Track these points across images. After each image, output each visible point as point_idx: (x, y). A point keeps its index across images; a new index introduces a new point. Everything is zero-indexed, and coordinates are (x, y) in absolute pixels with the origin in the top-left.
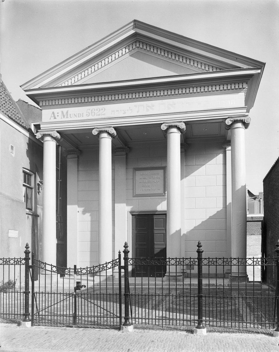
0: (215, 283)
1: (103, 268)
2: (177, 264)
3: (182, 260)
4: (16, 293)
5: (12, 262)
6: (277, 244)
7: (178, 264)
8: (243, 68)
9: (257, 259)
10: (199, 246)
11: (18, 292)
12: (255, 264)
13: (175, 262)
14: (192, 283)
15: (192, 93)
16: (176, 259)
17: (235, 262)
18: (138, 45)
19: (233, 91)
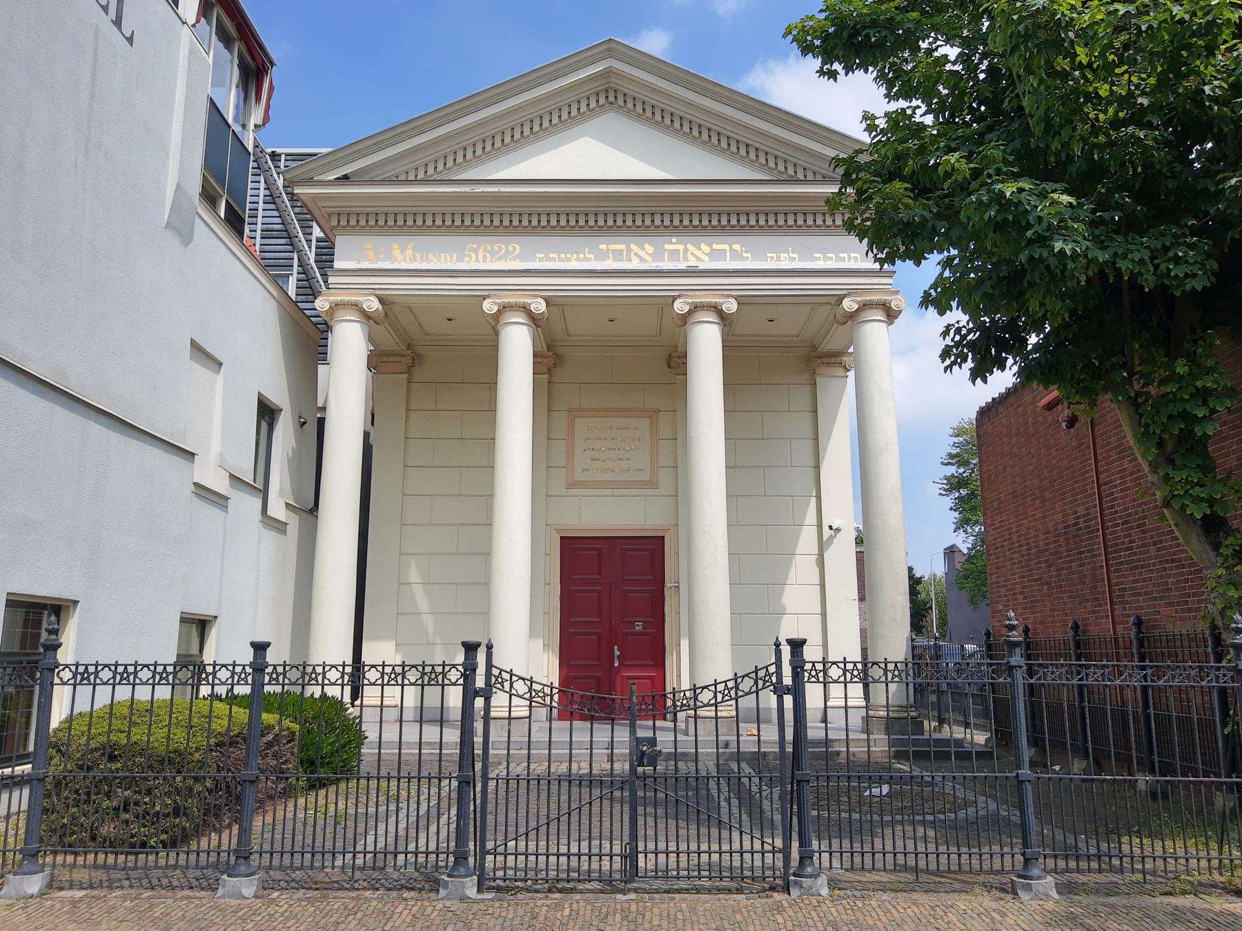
1: (726, 692)
2: (848, 680)
3: (439, 669)
5: (106, 675)
6: (1007, 622)
7: (851, 679)
13: (339, 675)
16: (234, 668)
17: (333, 675)
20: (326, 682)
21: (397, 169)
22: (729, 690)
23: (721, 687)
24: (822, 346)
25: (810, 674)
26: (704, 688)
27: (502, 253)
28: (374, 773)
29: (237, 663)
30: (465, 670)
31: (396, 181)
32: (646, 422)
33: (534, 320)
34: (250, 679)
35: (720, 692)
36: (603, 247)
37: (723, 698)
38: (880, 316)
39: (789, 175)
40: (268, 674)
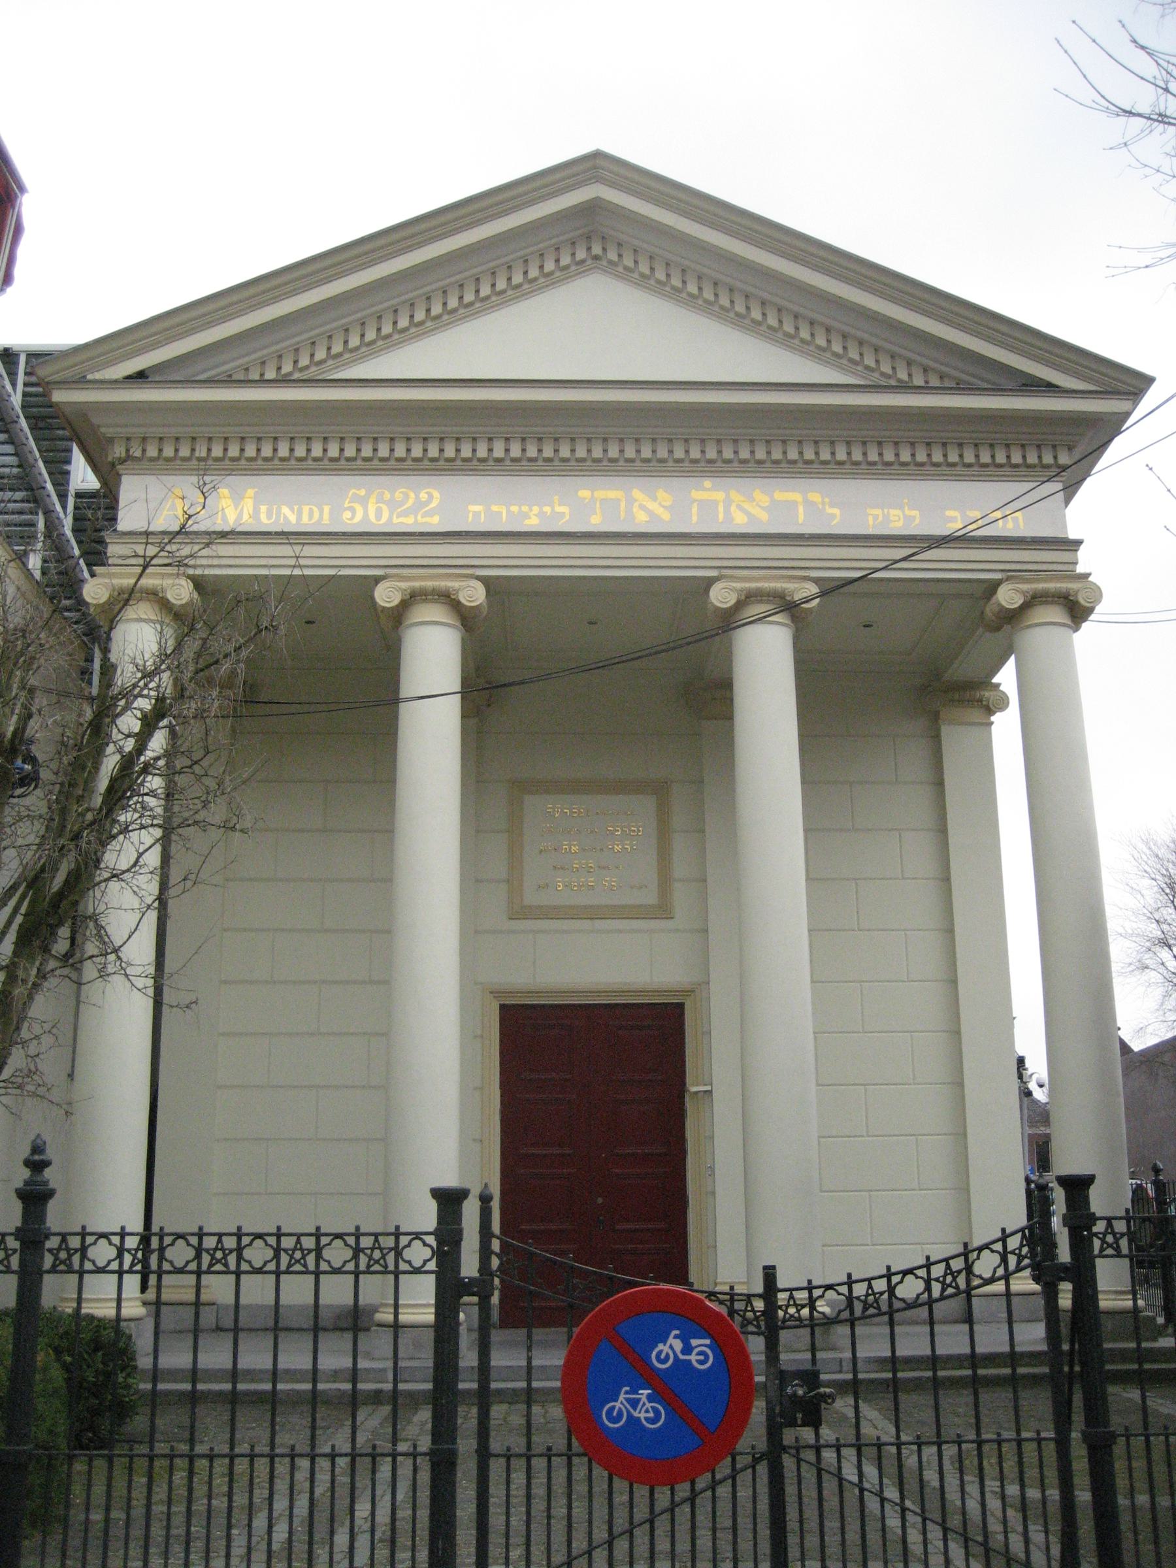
0: (305, 1363)
2: (363, 1267)
4: (323, 1464)
5: (258, 1254)
7: (369, 1266)
8: (969, 384)
9: (216, 1238)
10: (37, 1165)
11: (257, 1450)
12: (363, 1267)
13: (191, 1253)
14: (898, 1353)
15: (1035, 466)
18: (597, 250)
19: (965, 471)
20: (166, 1266)
21: (229, 364)
22: (955, 1275)
23: (938, 1271)
24: (950, 671)
25: (213, 1257)
26: (905, 1273)
27: (433, 505)
28: (385, 1446)
29: (402, 1230)
30: (440, 1243)
31: (229, 381)
32: (646, 805)
33: (466, 618)
34: (15, 1262)
35: (937, 1280)
36: (584, 494)
37: (943, 1290)
38: (1055, 614)
39: (899, 381)
40: (50, 1250)
